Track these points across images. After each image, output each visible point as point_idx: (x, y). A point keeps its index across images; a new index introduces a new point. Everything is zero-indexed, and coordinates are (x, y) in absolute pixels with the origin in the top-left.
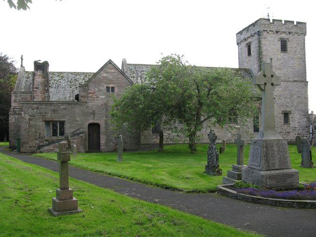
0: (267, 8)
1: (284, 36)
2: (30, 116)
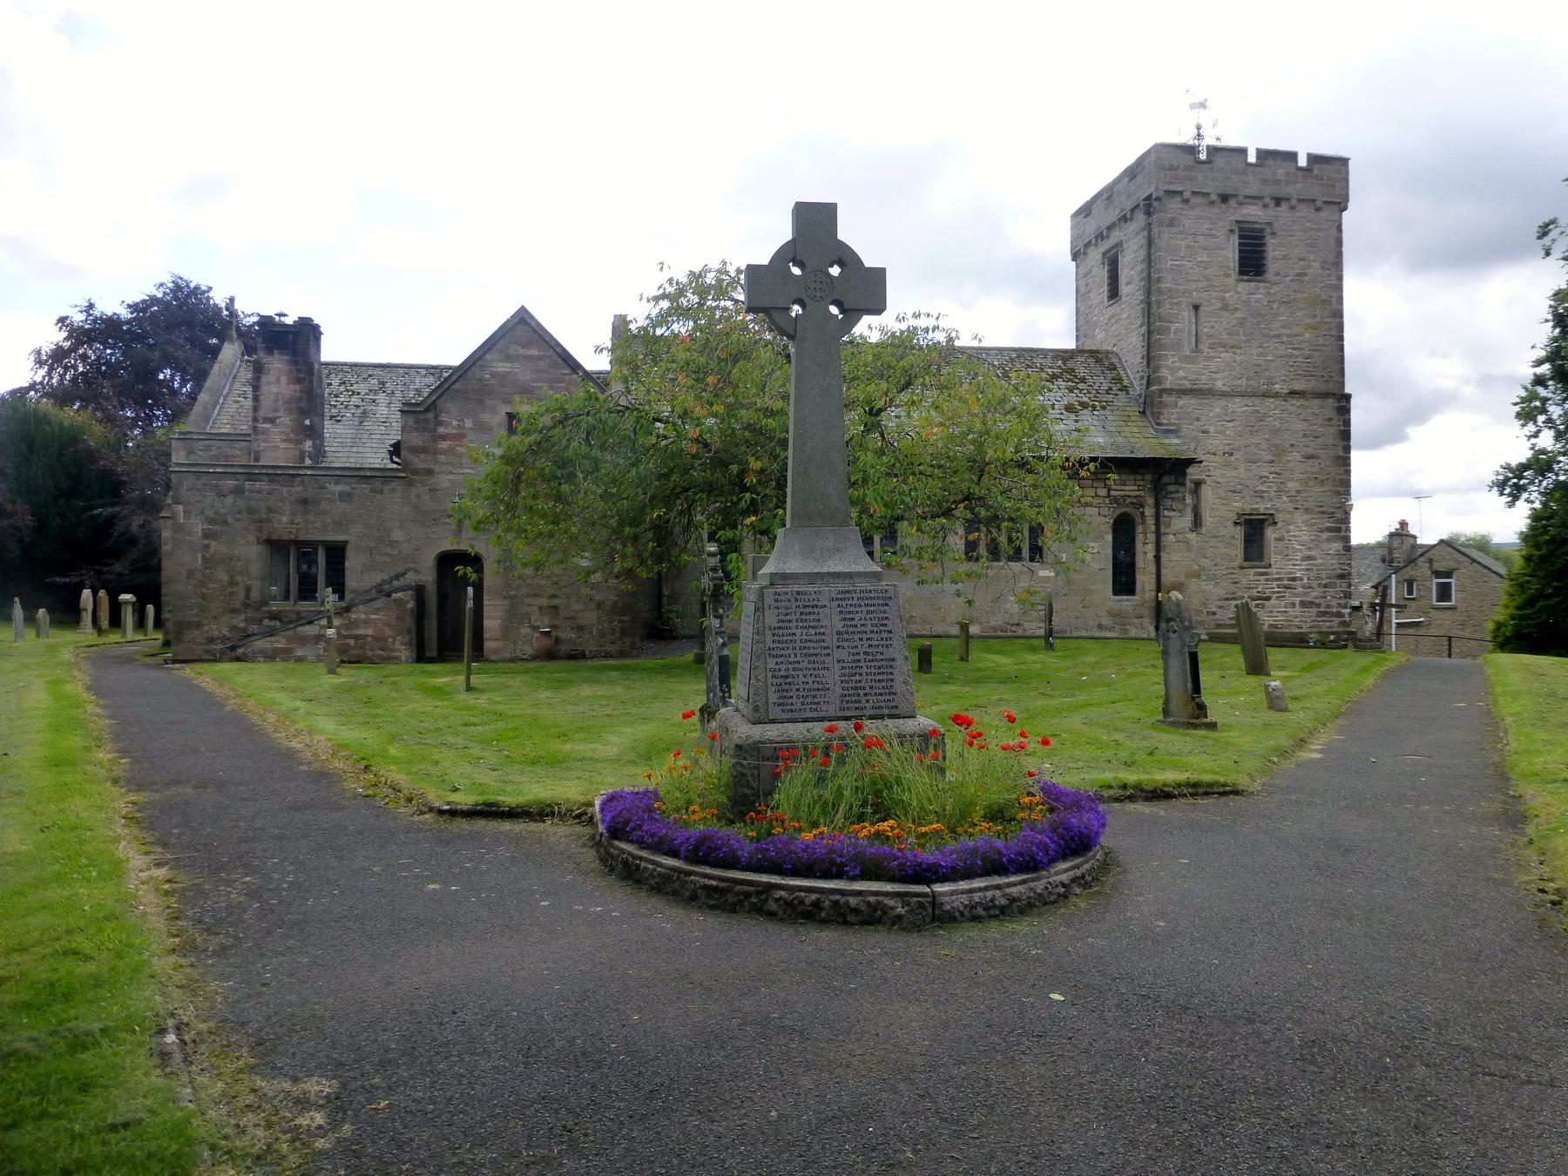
0: (1193, 106)
1: (1253, 213)
2: (211, 521)
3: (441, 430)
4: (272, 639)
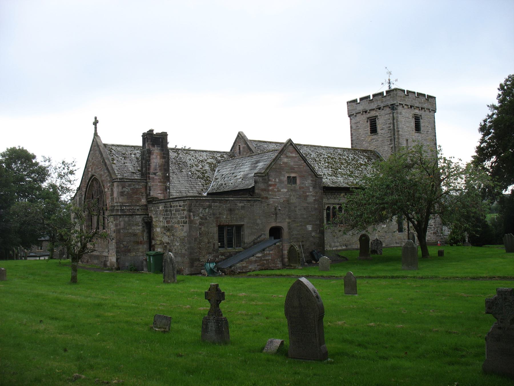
1: (417, 111)
2: (201, 218)
3: (270, 183)
4: (242, 263)
